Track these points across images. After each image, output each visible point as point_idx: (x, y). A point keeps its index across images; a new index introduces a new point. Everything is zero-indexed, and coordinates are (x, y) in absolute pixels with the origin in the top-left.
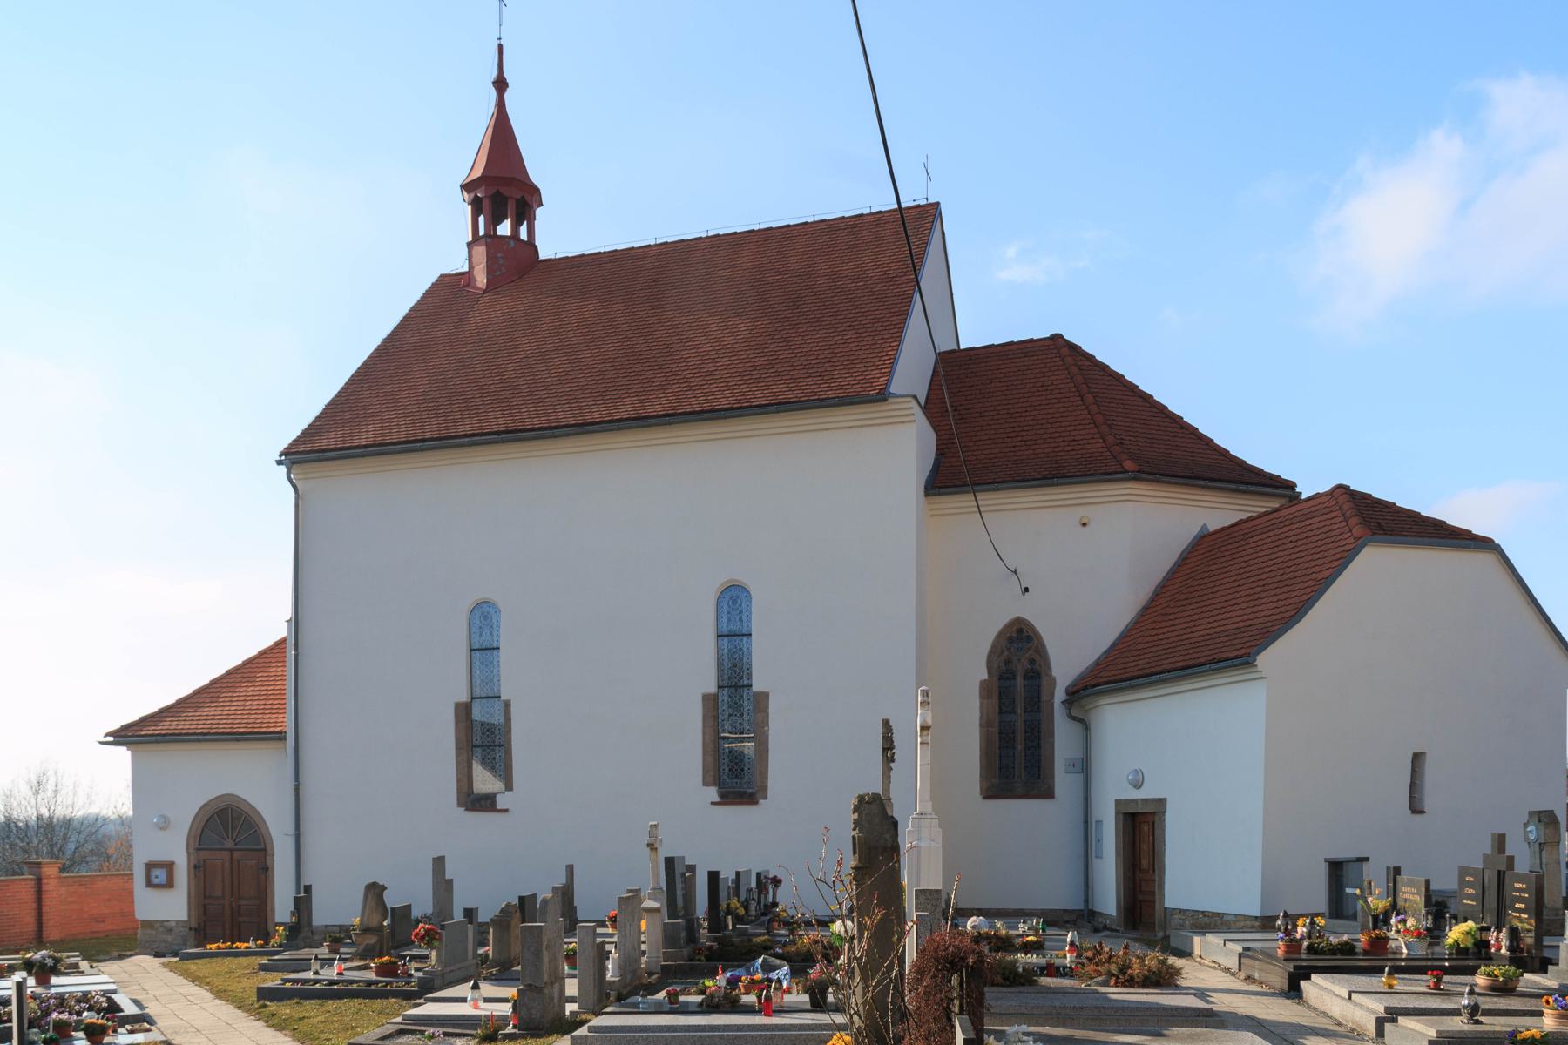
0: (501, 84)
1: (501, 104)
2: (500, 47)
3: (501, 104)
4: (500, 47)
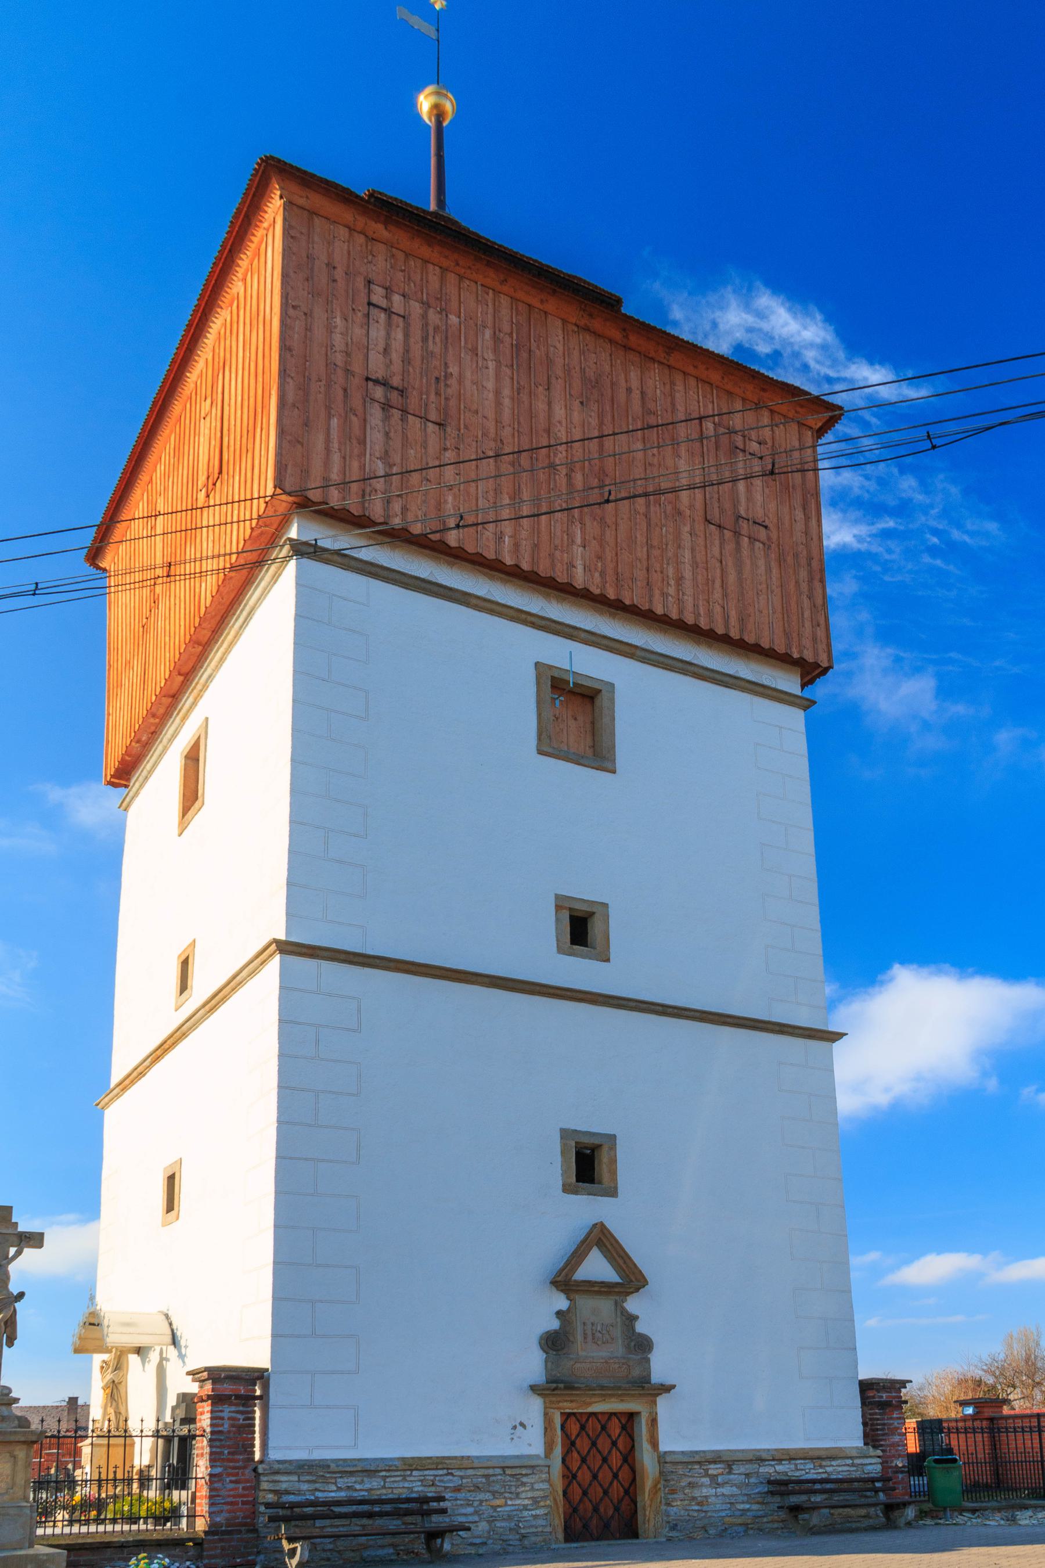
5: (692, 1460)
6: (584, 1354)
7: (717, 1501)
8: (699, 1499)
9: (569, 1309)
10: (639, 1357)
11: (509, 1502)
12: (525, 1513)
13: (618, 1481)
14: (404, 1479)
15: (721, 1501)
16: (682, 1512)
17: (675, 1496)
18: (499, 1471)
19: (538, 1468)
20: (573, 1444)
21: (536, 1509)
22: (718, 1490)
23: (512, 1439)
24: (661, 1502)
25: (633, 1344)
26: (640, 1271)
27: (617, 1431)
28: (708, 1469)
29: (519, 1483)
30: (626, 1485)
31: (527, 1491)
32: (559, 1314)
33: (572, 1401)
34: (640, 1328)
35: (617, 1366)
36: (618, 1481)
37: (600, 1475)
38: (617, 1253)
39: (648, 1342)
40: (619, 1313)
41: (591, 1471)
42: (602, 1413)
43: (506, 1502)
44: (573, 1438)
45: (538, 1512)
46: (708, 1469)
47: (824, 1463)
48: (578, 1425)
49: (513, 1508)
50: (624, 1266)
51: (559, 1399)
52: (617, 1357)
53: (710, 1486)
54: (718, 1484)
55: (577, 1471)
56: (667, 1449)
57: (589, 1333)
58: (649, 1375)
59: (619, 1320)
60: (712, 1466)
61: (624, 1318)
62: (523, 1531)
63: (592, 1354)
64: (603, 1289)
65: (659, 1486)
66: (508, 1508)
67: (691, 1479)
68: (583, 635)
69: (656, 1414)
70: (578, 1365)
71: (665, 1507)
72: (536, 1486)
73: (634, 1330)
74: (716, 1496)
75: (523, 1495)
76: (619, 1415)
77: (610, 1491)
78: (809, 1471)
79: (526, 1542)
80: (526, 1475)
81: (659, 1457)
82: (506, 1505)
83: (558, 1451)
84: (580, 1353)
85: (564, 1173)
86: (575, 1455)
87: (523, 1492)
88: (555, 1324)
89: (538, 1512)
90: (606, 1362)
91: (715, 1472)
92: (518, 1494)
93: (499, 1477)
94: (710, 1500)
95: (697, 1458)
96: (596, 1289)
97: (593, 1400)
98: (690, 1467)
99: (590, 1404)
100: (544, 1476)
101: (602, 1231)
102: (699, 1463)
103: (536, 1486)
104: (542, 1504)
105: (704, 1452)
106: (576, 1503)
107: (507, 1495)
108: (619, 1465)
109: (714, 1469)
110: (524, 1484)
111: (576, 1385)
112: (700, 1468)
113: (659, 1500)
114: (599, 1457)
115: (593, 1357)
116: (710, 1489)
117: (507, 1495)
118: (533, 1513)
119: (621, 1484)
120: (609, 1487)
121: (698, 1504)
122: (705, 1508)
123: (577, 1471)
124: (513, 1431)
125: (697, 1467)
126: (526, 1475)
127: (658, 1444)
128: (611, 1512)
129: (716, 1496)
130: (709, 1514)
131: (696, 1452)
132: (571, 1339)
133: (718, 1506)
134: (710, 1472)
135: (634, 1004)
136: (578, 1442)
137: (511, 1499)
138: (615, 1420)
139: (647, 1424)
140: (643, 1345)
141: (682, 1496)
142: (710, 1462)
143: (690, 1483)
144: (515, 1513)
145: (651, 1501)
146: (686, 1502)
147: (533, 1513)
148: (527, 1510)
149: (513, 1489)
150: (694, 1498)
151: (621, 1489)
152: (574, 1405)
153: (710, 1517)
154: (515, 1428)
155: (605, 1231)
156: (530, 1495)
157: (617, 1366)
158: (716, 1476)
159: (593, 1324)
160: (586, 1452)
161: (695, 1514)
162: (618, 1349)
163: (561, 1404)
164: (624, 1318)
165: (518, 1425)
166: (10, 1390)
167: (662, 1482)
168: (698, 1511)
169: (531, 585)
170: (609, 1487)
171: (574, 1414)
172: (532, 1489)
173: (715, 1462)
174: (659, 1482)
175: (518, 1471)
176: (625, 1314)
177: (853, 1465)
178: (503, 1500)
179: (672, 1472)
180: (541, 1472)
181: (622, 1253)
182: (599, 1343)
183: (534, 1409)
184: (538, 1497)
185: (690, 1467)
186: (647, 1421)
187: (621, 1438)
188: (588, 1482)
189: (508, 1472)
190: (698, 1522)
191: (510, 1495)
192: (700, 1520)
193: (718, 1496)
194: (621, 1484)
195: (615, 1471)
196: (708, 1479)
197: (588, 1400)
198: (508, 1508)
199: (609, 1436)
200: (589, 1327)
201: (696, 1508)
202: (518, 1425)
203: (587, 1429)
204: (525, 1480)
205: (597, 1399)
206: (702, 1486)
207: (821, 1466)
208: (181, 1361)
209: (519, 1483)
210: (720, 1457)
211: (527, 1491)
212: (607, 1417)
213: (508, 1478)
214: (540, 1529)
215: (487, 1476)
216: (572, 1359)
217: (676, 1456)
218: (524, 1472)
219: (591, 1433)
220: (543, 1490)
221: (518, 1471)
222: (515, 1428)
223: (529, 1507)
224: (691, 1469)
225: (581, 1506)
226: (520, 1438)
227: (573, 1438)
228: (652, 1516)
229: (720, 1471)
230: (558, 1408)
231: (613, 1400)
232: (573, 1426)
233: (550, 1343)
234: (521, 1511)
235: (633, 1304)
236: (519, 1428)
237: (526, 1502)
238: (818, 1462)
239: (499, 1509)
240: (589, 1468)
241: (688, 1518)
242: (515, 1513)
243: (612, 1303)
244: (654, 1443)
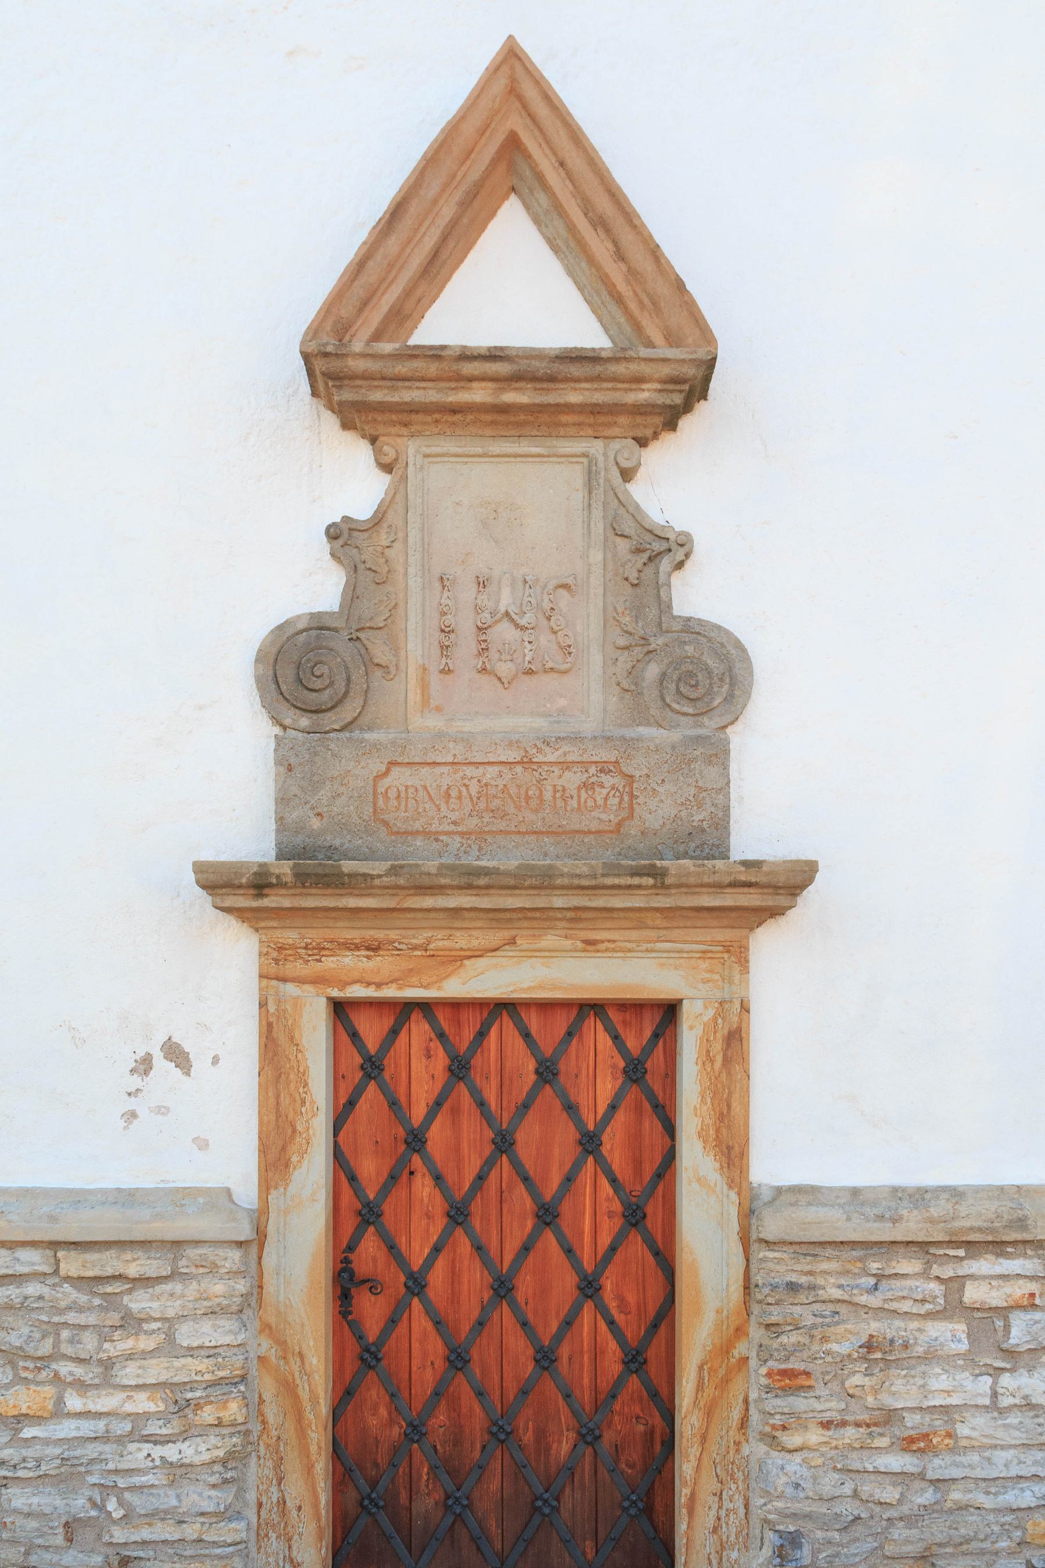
5: (885, 1233)
6: (434, 722)
7: (1005, 1437)
8: (912, 1420)
9: (379, 519)
10: (675, 736)
11: (74, 1402)
12: (138, 1454)
13: (602, 1309)
15: (1017, 1437)
16: (829, 1483)
17: (800, 1403)
18: (32, 1260)
19: (193, 1253)
20: (416, 1140)
21: (184, 1435)
22: (1006, 1380)
23: (133, 1115)
24: (744, 1423)
25: (652, 671)
26: (680, 286)
27: (607, 1087)
28: (961, 1280)
29: (114, 1318)
30: (633, 1331)
31: (145, 1355)
33: (374, 948)
35: (572, 779)
36: (602, 1309)
37: (525, 1286)
38: (587, 207)
39: (724, 658)
40: (599, 527)
41: (486, 1263)
42: (546, 1006)
43: (60, 1401)
44: (418, 1112)
45: (189, 1451)
46: (961, 1280)
48: (441, 1060)
49: (87, 1428)
50: (616, 273)
51: (315, 935)
52: (576, 739)
53: (969, 1359)
54: (1010, 1354)
55: (429, 1263)
57: (465, 625)
58: (722, 823)
59: (597, 556)
60: (984, 1265)
61: (623, 546)
62: (119, 1535)
63: (468, 727)
64: (510, 397)
65: (741, 1349)
66: (67, 1429)
67: (874, 1327)
69: (745, 1008)
70: (399, 778)
71: (761, 1449)
72: (186, 1335)
73: (665, 607)
75: (129, 1373)
76: (533, 1021)
77: (564, 1351)
81: (748, 1214)
82: (59, 1412)
84: (417, 721)
86: (423, 1188)
87: (130, 1357)
89: (189, 1451)
90: (527, 763)
91: (996, 1297)
92: (108, 1365)
93: (32, 1289)
94: (962, 1430)
95: (912, 1227)
96: (479, 394)
97: (462, 941)
98: (874, 1266)
99: (456, 959)
100: (219, 1288)
101: (513, 91)
102: (921, 1247)
103: (186, 1335)
104: (208, 1415)
105: (956, 1194)
106: (417, 1405)
107: (65, 1368)
108: (605, 1240)
110: (132, 1323)
111: (348, 866)
112: (925, 1275)
113: (736, 1414)
114: (522, 1200)
115: (467, 740)
116: (965, 1378)
117: (65, 1368)
118: (171, 1452)
119: (611, 1323)
120: (558, 1338)
121: (909, 1444)
122: (939, 1466)
123: (429, 1263)
124: (136, 1081)
127: (744, 1154)
128: (563, 1447)
129: (994, 1407)
130: (956, 1495)
131: (920, 1196)
132: (380, 653)
133: (1001, 1457)
134: (972, 1293)
136: (437, 1135)
137: (81, 1386)
138: (419, 1030)
139: (708, 1058)
141: (831, 1407)
142: (973, 1248)
143: (869, 1346)
144: (91, 1450)
145: (709, 1412)
146: (850, 1434)
147: (171, 1452)
148: (147, 1439)
149: (89, 1342)
150: (889, 1417)
151: (613, 1345)
152: (382, 964)
153: (962, 1508)
154: (144, 1066)
155: (531, 93)
156: (157, 1371)
157: (572, 779)
158: (1003, 1312)
159: (482, 584)
160: (555, 1181)
161: (890, 1494)
163: (330, 963)
164: (623, 546)
165: (158, 1057)
167: (756, 1333)
168: (901, 1477)
170: (558, 1338)
171: (425, 1007)
172: (170, 1347)
173: (998, 1247)
174: (740, 1331)
175: (110, 1263)
176: (628, 527)
178: (49, 1391)
179: (793, 1287)
180: (213, 1269)
181: (604, 205)
182: (505, 669)
184: (190, 1385)
185: (874, 1266)
186: (706, 1042)
187: (621, 1116)
188: (469, 1311)
189: (72, 1264)
190: (898, 1533)
191: (79, 1371)
192: (910, 1520)
193: (1002, 1412)
194: (611, 1323)
195: (588, 1264)
196: (961, 1328)
197: (440, 942)
198: (67, 1429)
199: (571, 1108)
200: (467, 594)
201: (897, 1462)
202: (158, 1057)
203: (476, 1077)
204: (139, 1302)
205: (479, 939)
206: (930, 1357)
209: (114, 1318)
210: (1021, 1223)
211: (145, 1355)
212: (561, 1023)
213: (69, 1293)
214: (191, 1531)
216: (376, 746)
217: (814, 1213)
218: (133, 1271)
219: (491, 1097)
220: (212, 1352)
221: (110, 1263)
222: (144, 1066)
223: (153, 1428)
224: (879, 1277)
225: (441, 1417)
226: (162, 1110)
227: (418, 1112)
228: (708, 1485)
229: (1020, 1290)
230: (319, 980)
231: (549, 940)
232: (418, 1065)
233: (287, 674)
234: (121, 1440)
236: (162, 1065)
237: (142, 1403)
239: (28, 1433)
240: (479, 1249)
241: (848, 1509)
242: (91, 1450)
243: (576, 474)
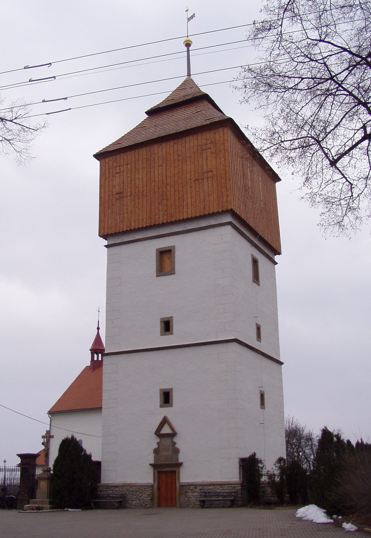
0: (98, 329)
1: (98, 332)
2: (98, 321)
3: (98, 332)
4: (98, 321)
14: (122, 489)
32: (158, 443)
34: (177, 446)
47: (223, 486)
56: (182, 482)
66: (143, 497)
68: (166, 235)
74: (192, 495)
78: (219, 489)
79: (147, 506)
80: (147, 488)
83: (156, 482)
85: (160, 401)
88: (156, 446)
92: (145, 493)
104: (150, 496)
109: (192, 487)
125: (187, 487)
126: (147, 488)
134: (191, 488)
135: (248, 238)
140: (176, 451)
162: (170, 452)
166: (280, 460)
169: (189, 97)
177: (231, 487)
183: (151, 471)
198: (143, 497)
207: (222, 487)
208: (100, 327)
213: (143, 489)
215: (139, 488)
235: (175, 440)
238: (221, 486)
244: (179, 479)
